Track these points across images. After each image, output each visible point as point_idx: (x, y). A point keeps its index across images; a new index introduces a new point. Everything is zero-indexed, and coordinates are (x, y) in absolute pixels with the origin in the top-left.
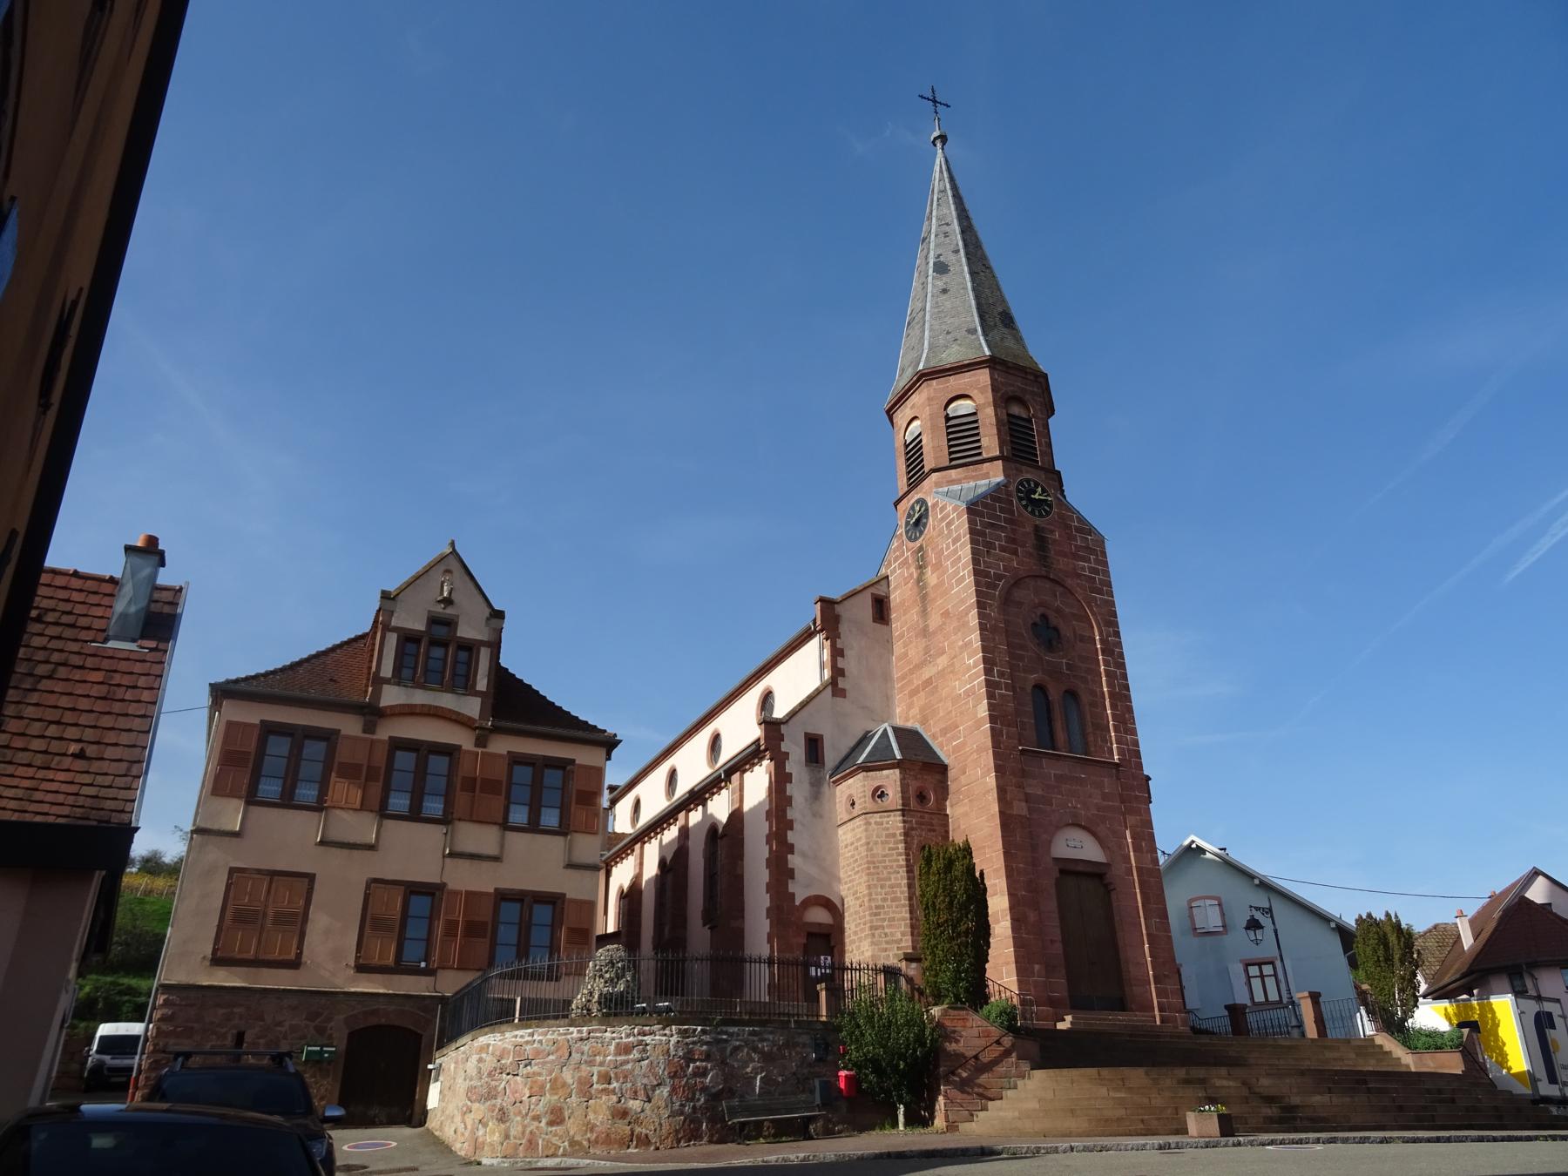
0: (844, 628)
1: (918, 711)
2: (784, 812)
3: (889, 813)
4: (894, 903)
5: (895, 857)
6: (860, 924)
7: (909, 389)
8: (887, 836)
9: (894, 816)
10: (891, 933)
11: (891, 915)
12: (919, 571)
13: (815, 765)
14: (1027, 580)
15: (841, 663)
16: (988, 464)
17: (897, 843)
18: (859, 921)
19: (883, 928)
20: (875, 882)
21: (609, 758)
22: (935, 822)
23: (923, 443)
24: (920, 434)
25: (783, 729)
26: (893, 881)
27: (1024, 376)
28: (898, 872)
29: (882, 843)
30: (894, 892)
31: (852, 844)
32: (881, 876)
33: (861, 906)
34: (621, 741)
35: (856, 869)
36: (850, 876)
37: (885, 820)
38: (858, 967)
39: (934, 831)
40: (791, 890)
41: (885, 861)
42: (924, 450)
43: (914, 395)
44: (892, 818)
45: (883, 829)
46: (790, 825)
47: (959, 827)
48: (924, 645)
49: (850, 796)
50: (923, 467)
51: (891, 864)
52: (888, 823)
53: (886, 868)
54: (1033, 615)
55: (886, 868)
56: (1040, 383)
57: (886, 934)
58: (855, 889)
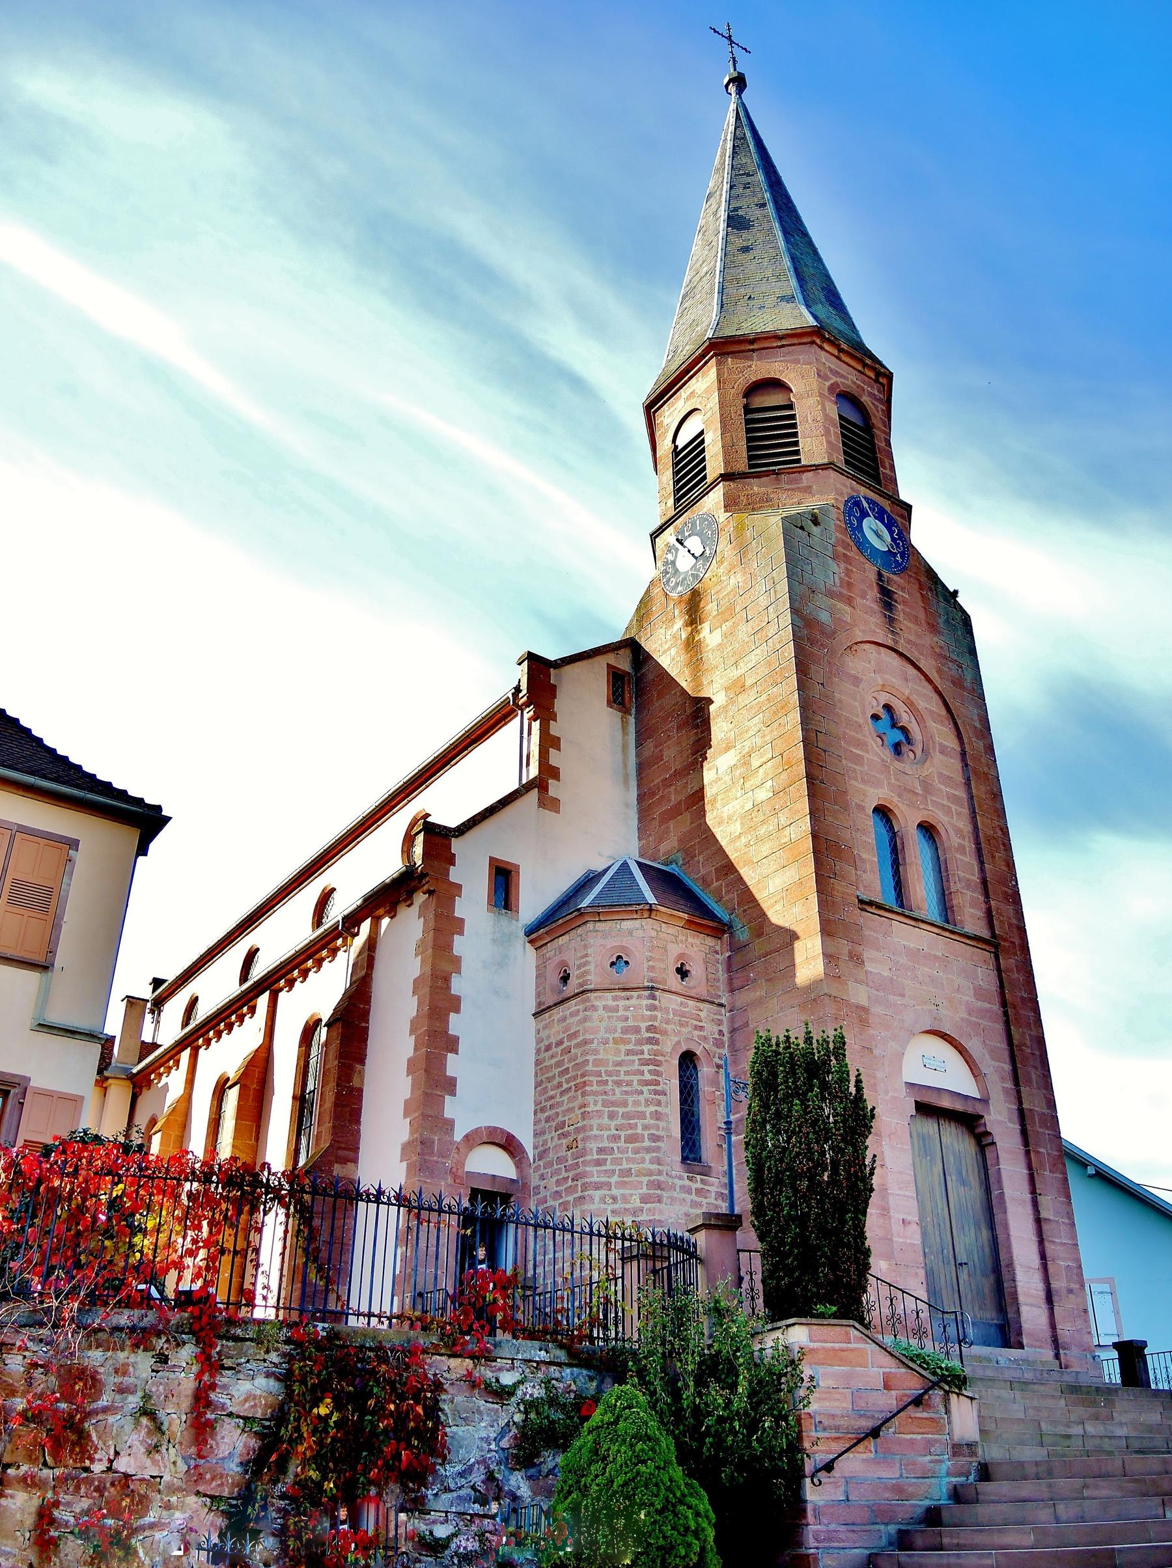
0: (561, 705)
1: (675, 844)
2: (447, 980)
3: (628, 993)
4: (631, 1146)
5: (636, 1067)
6: (566, 1179)
7: (687, 371)
8: (625, 1031)
9: (639, 997)
10: (623, 1195)
11: (625, 1166)
12: (689, 629)
13: (504, 911)
14: (867, 646)
15: (554, 758)
16: (811, 474)
17: (642, 1044)
18: (564, 1174)
19: (608, 1185)
20: (599, 1107)
21: (143, 850)
22: (703, 1015)
23: (705, 445)
24: (702, 433)
25: (456, 845)
26: (630, 1108)
27: (860, 368)
28: (642, 1093)
29: (615, 1041)
30: (632, 1127)
31: (560, 1043)
32: (611, 1098)
33: (569, 1148)
34: (169, 819)
35: (565, 1086)
36: (552, 1097)
37: (622, 1003)
38: (603, 1232)
39: (701, 1028)
40: (447, 1114)
41: (618, 1073)
42: (707, 454)
43: (694, 380)
44: (633, 1002)
45: (619, 1019)
46: (455, 1004)
47: (746, 1024)
48: (693, 739)
49: (564, 964)
50: (705, 477)
51: (627, 1078)
52: (627, 1008)
53: (618, 1083)
54: (875, 703)
55: (618, 1083)
56: (882, 385)
57: (614, 1199)
58: (560, 1119)
